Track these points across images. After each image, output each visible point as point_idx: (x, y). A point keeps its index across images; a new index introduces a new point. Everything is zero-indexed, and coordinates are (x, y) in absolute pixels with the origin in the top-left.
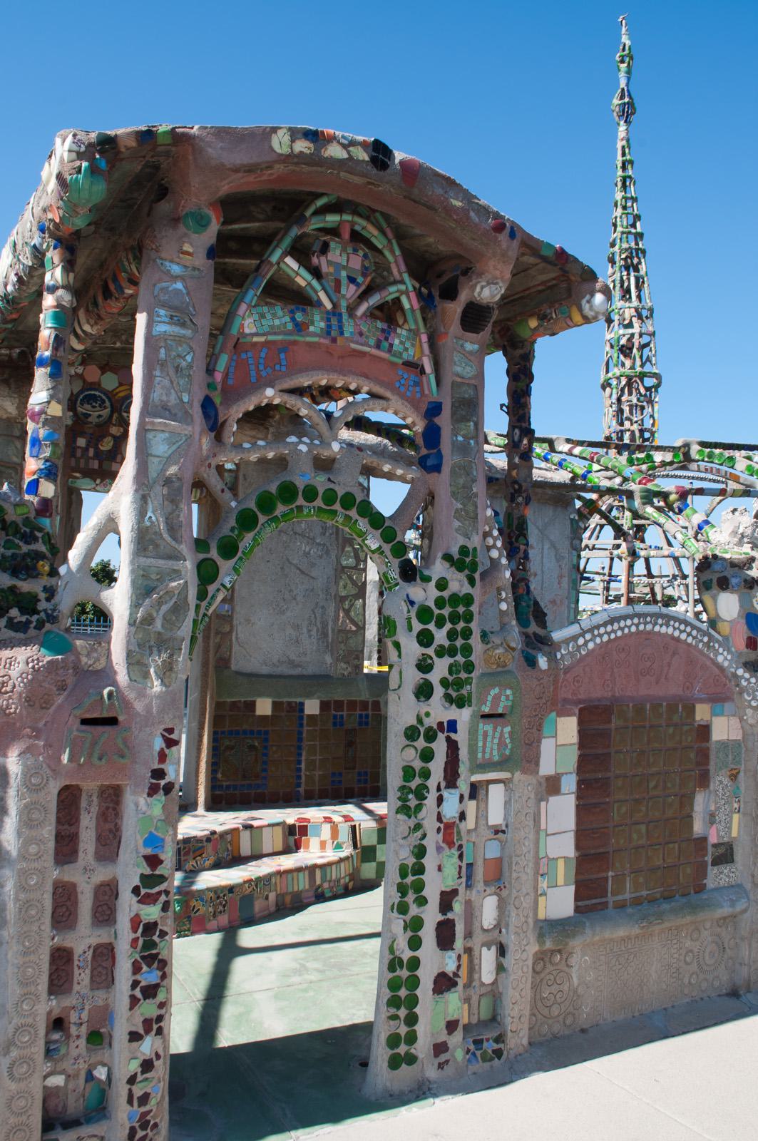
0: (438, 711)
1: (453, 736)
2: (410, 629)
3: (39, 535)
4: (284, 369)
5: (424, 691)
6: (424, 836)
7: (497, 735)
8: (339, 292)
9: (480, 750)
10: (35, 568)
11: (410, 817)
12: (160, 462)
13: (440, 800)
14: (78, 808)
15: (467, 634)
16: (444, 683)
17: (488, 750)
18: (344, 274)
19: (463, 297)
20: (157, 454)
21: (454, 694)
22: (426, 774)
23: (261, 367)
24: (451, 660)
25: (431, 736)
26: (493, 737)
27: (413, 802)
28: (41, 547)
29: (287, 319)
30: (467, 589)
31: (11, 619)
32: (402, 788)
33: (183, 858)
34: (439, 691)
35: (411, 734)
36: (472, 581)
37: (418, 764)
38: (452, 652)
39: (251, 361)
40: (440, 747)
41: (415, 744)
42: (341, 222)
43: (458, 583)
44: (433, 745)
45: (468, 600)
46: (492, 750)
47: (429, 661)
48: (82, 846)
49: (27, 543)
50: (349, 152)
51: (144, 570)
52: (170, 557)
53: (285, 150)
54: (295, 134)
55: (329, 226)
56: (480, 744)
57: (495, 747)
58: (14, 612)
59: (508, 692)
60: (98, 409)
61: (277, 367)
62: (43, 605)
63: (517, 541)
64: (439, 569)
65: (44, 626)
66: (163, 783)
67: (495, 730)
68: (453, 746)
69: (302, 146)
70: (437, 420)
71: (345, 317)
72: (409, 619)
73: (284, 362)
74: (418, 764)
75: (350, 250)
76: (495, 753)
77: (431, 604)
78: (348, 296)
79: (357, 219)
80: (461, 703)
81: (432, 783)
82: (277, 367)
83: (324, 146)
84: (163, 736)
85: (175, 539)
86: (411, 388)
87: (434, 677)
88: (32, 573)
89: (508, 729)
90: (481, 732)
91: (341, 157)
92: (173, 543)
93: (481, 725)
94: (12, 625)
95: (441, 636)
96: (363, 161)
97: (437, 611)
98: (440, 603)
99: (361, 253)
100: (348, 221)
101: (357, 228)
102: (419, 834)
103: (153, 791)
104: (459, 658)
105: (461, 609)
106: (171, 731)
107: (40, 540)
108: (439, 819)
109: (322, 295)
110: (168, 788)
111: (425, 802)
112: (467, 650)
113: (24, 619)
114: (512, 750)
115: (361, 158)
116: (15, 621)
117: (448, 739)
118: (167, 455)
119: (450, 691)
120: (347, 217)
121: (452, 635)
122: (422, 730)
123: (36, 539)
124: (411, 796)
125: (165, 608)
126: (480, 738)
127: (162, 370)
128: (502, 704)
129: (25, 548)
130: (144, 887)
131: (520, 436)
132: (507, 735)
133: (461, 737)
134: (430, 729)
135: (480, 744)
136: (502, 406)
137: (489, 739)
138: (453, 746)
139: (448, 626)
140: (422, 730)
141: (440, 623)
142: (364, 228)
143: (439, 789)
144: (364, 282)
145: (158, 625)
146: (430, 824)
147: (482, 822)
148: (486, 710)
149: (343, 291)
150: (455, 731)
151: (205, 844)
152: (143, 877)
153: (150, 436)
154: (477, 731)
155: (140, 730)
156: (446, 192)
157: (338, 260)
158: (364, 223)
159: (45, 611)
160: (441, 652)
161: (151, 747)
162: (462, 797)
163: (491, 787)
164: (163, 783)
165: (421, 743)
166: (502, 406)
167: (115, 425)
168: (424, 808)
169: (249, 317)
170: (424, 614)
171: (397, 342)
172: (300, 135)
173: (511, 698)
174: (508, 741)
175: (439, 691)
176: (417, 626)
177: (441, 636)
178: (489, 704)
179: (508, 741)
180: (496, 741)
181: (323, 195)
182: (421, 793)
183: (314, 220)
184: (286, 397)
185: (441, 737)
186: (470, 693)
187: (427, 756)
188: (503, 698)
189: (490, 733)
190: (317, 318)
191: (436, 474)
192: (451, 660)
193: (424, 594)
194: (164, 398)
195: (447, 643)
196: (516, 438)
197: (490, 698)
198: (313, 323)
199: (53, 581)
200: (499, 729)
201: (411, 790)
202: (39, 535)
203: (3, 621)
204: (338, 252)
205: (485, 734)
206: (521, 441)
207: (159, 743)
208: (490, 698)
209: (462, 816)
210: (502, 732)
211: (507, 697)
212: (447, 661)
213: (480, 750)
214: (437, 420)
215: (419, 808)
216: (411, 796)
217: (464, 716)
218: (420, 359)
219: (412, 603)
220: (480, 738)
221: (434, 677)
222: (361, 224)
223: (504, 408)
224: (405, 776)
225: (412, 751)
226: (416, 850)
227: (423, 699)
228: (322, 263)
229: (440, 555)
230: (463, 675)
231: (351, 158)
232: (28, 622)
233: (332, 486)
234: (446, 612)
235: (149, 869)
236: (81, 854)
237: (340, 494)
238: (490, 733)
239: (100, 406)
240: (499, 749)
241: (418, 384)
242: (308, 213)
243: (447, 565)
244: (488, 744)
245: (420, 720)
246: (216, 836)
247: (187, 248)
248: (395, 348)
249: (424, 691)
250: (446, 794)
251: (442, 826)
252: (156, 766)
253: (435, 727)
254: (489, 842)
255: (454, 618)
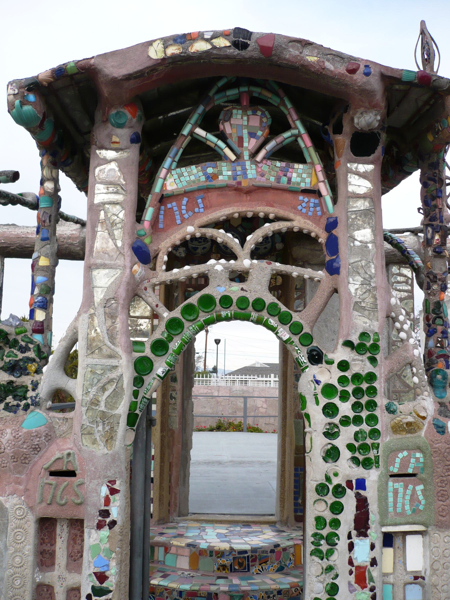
0: (346, 469)
1: (362, 492)
2: (317, 403)
3: (31, 346)
4: (202, 210)
5: (332, 454)
6: (337, 576)
7: (409, 492)
8: (242, 146)
9: (391, 504)
10: (26, 369)
11: (322, 559)
12: (102, 291)
13: (351, 547)
14: (55, 535)
15: (372, 405)
16: (350, 447)
17: (399, 505)
18: (245, 132)
19: (346, 128)
20: (100, 285)
21: (361, 458)
22: (336, 523)
23: (184, 212)
24: (357, 429)
25: (339, 491)
26: (405, 494)
27: (324, 547)
28: (31, 354)
29: (201, 174)
30: (368, 368)
31: (7, 404)
32: (315, 535)
33: (250, 564)
34: (345, 454)
35: (322, 489)
36: (373, 360)
37: (328, 516)
38: (357, 420)
39: (175, 209)
40: (349, 502)
41: (325, 498)
42: (240, 94)
43: (360, 365)
44: (343, 500)
45: (371, 377)
46: (403, 505)
47: (336, 430)
48: (57, 561)
49: (22, 352)
50: (212, 44)
51: (91, 368)
52: (110, 357)
53: (161, 55)
54: (166, 42)
55: (231, 98)
56: (391, 499)
57: (407, 502)
58: (10, 399)
59: (418, 455)
60: (203, 243)
61: (196, 210)
62: (30, 394)
63: (434, 322)
64: (341, 354)
65: (29, 408)
66: (108, 520)
67: (406, 487)
68: (362, 503)
69: (173, 50)
70: (334, 232)
71: (248, 163)
72: (315, 395)
73: (201, 206)
74: (328, 516)
75: (249, 112)
76: (407, 507)
77: (335, 382)
78: (250, 148)
79: (253, 89)
80: (367, 464)
81: (343, 531)
82: (196, 210)
83: (191, 45)
84: (108, 486)
85: (114, 344)
86: (312, 209)
87: (341, 443)
88: (24, 371)
89: (421, 487)
90: (391, 489)
91: (205, 49)
92: (113, 347)
93: (390, 484)
94: (7, 408)
95: (345, 409)
96: (226, 47)
97: (340, 388)
98: (342, 380)
99: (259, 113)
100: (245, 92)
101: (255, 95)
102: (332, 574)
103: (100, 526)
104: (365, 427)
105: (365, 386)
106: (113, 482)
107: (32, 350)
108: (351, 562)
109: (227, 151)
110: (113, 523)
111: (337, 547)
112: (372, 419)
113: (15, 403)
114: (425, 505)
115: (223, 45)
116: (10, 405)
117: (358, 495)
118: (107, 286)
119: (357, 455)
120: (244, 89)
121: (356, 406)
122: (331, 487)
123: (29, 349)
124: (323, 542)
125: (107, 393)
126: (391, 495)
127: (102, 227)
128: (411, 465)
129: (21, 356)
130: (94, 596)
131: (433, 232)
132: (419, 493)
133: (371, 493)
134: (338, 486)
135: (391, 499)
136: (419, 209)
137: (400, 495)
138: (362, 503)
139: (353, 400)
140: (331, 487)
141: (344, 397)
142: (260, 94)
143: (349, 537)
144: (262, 135)
145: (102, 407)
146: (342, 567)
147: (399, 567)
148: (396, 471)
149: (245, 144)
150: (364, 489)
151: (269, 554)
152: (93, 588)
153: (95, 273)
154: (386, 489)
155: (90, 482)
156: (301, 53)
157: (240, 122)
158: (258, 90)
159: (31, 397)
160: (345, 421)
161: (99, 495)
162: (372, 547)
163: (409, 538)
164: (108, 520)
165: (330, 499)
166: (419, 209)
167: (214, 253)
168: (336, 552)
169: (170, 178)
170: (329, 390)
171: (294, 175)
172: (171, 42)
173: (422, 460)
174: (421, 497)
175: (345, 454)
176: (323, 401)
177: (345, 409)
178: (397, 465)
179: (421, 497)
180: (408, 497)
181: (220, 78)
182: (331, 540)
183: (216, 97)
184: (204, 230)
185: (350, 494)
186: (377, 457)
187: (337, 508)
188: (413, 460)
189: (401, 490)
190: (224, 169)
191: (337, 275)
192: (357, 429)
193: (329, 375)
194: (105, 246)
195: (351, 414)
196: (429, 236)
197: (398, 460)
198: (221, 174)
199: (37, 377)
200: (411, 487)
201: (322, 537)
202: (31, 346)
203: (2, 405)
204: (239, 117)
205: (396, 492)
206: (433, 237)
207: (104, 491)
208: (398, 460)
209: (374, 562)
210: (414, 490)
211: (417, 459)
212: (353, 429)
213: (391, 504)
214: (334, 232)
215: (330, 553)
216: (323, 542)
217: (372, 477)
218: (317, 184)
219: (318, 382)
220: (391, 495)
221: (341, 443)
222: (256, 91)
223: (421, 211)
224: (317, 525)
225: (324, 504)
226: (329, 587)
227: (330, 461)
228: (227, 128)
229: (341, 341)
230: (369, 441)
231: (214, 47)
232: (18, 406)
233: (243, 294)
234: (350, 388)
235: (98, 582)
236: (56, 567)
237: (251, 300)
238: (401, 490)
239: (204, 241)
240: (411, 505)
241: (320, 204)
242: (211, 94)
243: (348, 349)
244: (400, 500)
245: (328, 479)
246: (279, 549)
247: (115, 139)
248: (293, 180)
249: (332, 454)
250: (356, 540)
251: (353, 569)
252: (103, 508)
253: (344, 485)
254: (409, 587)
255: (358, 392)
